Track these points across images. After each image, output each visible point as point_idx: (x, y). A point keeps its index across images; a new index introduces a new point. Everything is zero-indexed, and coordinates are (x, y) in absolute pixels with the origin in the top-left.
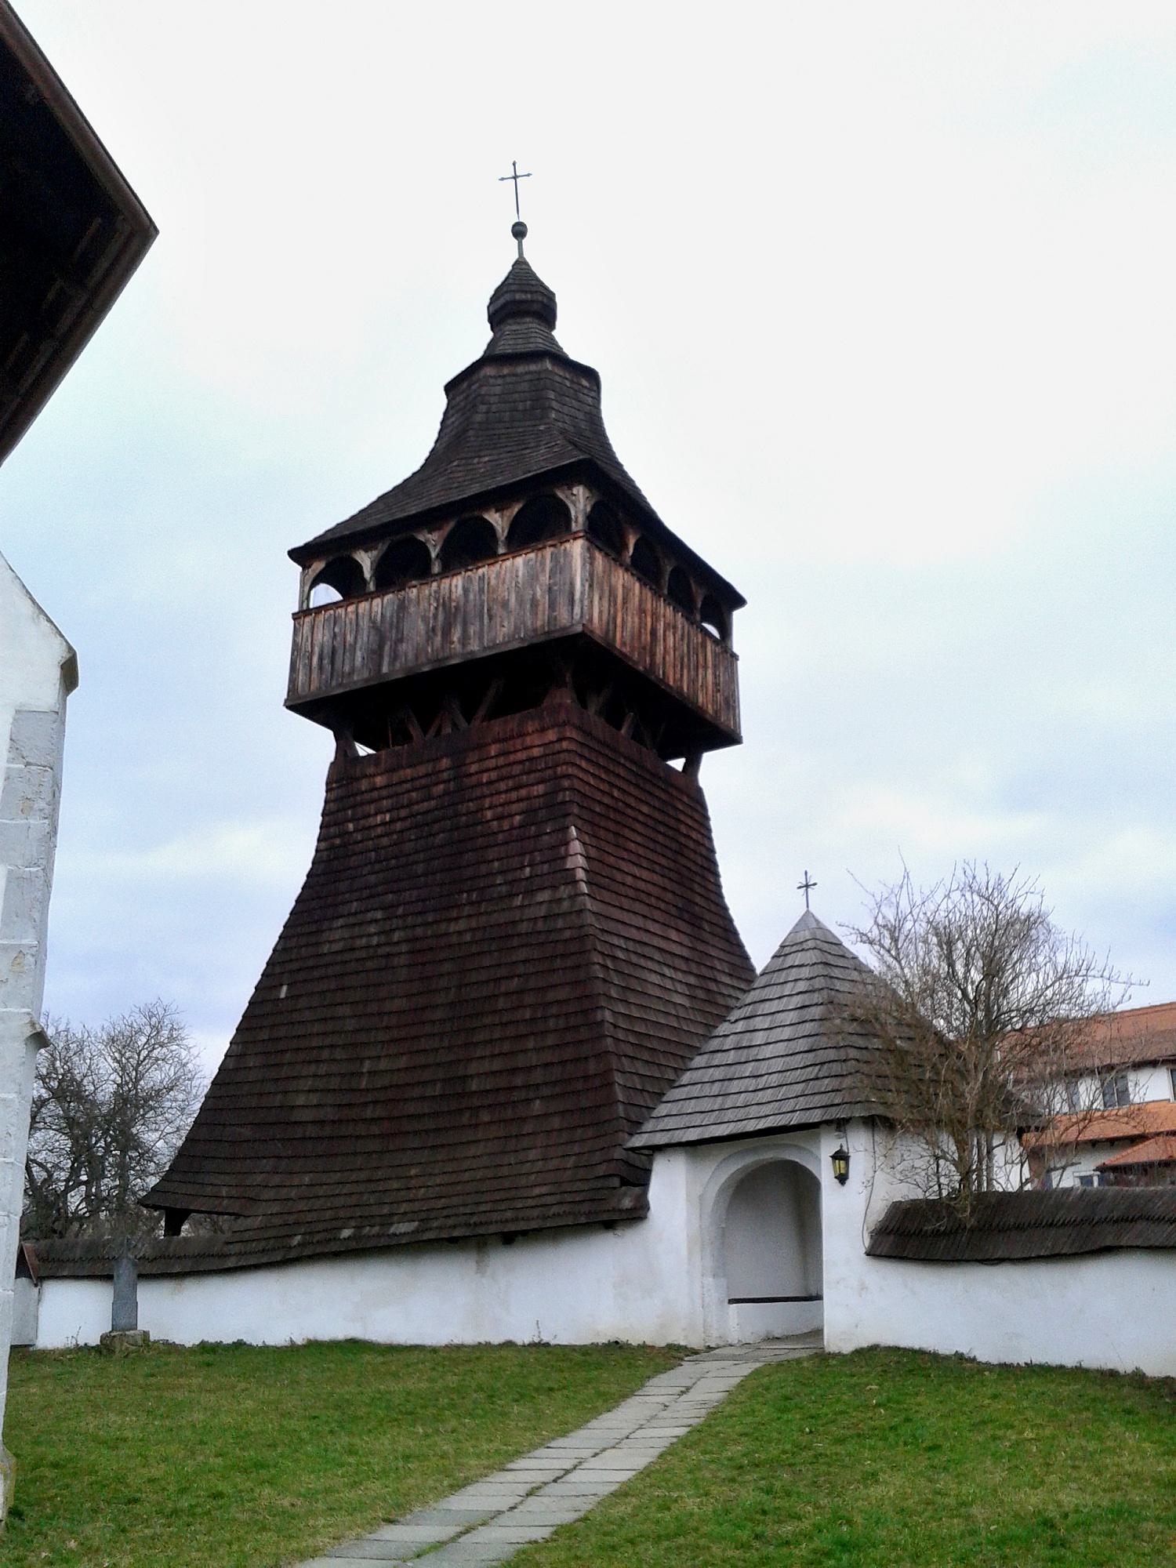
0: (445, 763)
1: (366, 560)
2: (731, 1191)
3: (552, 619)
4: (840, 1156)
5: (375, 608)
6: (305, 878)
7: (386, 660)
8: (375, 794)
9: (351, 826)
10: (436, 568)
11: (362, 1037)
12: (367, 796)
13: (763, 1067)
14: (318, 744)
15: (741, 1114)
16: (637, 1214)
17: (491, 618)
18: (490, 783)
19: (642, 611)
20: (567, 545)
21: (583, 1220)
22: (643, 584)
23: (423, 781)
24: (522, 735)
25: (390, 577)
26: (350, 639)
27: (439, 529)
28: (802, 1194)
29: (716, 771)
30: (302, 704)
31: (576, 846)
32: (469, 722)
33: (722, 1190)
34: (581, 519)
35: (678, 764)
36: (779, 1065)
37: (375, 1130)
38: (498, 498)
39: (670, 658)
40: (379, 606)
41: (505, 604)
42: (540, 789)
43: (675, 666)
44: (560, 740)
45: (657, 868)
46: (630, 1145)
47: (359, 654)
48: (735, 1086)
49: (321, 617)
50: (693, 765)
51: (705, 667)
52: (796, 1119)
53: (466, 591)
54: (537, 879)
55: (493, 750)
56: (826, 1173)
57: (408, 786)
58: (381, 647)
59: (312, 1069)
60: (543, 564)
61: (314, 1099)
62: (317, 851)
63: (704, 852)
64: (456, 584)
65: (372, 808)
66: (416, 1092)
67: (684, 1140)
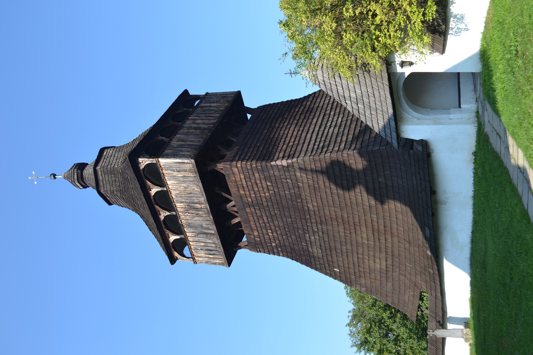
0: (248, 210)
1: (172, 238)
2: (416, 107)
3: (190, 171)
4: (403, 64)
5: (190, 235)
6: (294, 261)
7: (209, 231)
8: (261, 235)
9: (274, 244)
10: (174, 213)
11: (354, 243)
12: (262, 238)
13: (365, 94)
14: (243, 255)
15: (384, 104)
16: (424, 144)
17: (191, 193)
18: (255, 193)
19: (187, 134)
20: (161, 164)
21: (426, 166)
22: (177, 133)
23: (255, 218)
24: (236, 181)
25: (178, 229)
26: (202, 244)
27: (159, 211)
28: (419, 79)
29: (251, 101)
30: (229, 258)
31: (279, 162)
32: (232, 201)
33: (415, 111)
34: (151, 160)
35: (249, 116)
36: (364, 89)
37: (389, 240)
38: (145, 191)
39: (207, 122)
40: (189, 234)
41: (185, 188)
42: (257, 175)
43: (209, 120)
44: (237, 167)
45: (288, 127)
46: (397, 148)
47: (208, 241)
48: (373, 105)
49: (195, 254)
50: (249, 110)
51: (210, 106)
52: (386, 82)
53: (181, 202)
54: (292, 177)
55: (242, 192)
56: (407, 71)
57: (257, 224)
58: (205, 233)
59: (366, 261)
60: (168, 174)
61: (378, 261)
62: (283, 256)
63: (282, 107)
64: (179, 206)
65: (266, 236)
66: (376, 224)
67: (395, 127)
